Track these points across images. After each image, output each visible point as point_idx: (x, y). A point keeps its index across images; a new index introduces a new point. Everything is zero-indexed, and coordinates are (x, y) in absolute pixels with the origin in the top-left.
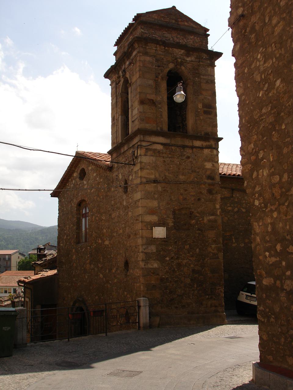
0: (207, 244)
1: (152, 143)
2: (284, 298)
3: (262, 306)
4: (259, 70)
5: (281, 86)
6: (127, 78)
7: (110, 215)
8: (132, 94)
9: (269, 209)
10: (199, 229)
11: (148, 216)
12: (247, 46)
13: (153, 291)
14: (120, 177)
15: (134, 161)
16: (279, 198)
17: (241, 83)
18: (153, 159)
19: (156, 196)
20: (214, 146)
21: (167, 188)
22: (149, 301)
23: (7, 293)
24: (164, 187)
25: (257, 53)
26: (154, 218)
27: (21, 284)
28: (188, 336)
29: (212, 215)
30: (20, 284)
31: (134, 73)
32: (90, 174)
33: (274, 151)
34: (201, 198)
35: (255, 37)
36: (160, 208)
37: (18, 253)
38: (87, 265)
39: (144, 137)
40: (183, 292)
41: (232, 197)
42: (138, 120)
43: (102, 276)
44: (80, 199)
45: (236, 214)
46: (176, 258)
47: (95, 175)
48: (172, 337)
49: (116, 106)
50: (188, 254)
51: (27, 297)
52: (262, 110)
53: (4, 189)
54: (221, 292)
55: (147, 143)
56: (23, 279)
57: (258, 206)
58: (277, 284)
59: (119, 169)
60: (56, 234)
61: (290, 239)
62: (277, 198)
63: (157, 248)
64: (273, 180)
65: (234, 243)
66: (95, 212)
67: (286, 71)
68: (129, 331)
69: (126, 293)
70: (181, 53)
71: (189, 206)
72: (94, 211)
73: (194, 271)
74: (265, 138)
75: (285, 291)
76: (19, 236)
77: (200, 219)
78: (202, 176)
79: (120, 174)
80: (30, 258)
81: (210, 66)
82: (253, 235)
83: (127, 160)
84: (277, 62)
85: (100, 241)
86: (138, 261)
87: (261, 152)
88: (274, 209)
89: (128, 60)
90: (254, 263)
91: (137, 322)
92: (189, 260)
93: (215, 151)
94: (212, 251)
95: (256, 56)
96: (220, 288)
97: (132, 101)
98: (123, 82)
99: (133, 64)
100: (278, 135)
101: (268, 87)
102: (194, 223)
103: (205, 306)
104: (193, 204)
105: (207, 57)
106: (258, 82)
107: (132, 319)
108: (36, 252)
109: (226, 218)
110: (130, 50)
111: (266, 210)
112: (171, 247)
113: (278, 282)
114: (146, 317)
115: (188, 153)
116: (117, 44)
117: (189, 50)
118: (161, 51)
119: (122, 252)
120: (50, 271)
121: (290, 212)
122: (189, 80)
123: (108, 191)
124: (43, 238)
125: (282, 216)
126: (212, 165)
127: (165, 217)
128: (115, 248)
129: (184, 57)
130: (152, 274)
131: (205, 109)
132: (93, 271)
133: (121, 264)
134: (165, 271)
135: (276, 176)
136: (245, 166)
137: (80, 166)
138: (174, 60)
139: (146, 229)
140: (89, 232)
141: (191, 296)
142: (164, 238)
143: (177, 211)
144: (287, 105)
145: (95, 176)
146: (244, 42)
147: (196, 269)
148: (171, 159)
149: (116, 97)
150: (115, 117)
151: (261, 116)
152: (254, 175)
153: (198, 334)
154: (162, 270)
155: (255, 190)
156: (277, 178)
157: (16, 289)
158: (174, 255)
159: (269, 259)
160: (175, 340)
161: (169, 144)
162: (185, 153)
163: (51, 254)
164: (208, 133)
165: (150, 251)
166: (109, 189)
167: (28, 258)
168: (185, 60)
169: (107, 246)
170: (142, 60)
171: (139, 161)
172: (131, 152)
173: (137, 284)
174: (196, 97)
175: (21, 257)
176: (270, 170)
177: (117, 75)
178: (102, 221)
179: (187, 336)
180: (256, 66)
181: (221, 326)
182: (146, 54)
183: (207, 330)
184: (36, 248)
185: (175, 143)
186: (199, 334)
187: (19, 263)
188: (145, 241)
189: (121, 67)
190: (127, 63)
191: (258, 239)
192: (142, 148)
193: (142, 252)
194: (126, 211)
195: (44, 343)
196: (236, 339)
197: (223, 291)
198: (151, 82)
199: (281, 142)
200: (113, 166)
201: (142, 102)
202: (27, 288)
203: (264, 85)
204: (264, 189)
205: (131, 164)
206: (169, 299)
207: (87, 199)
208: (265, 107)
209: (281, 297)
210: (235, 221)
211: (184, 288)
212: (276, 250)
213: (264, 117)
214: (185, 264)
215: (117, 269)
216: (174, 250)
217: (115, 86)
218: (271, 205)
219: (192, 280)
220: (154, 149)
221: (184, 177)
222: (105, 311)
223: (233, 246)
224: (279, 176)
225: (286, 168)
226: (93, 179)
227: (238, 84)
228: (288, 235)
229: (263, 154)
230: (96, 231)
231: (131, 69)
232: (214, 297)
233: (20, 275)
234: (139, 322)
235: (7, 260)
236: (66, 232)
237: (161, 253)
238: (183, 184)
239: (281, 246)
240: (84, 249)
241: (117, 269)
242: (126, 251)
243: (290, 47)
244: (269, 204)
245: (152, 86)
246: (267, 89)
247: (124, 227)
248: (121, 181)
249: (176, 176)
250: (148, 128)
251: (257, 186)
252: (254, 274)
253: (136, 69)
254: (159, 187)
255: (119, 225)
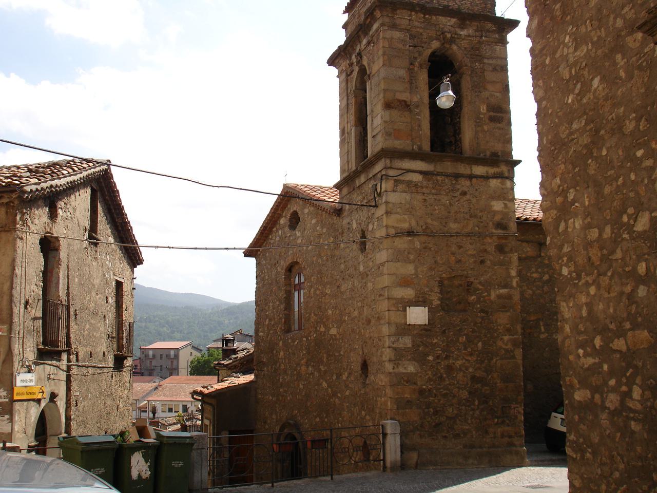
0: (496, 334)
1: (405, 171)
2: (606, 421)
3: (573, 433)
4: (567, 61)
5: (600, 88)
6: (364, 65)
7: (338, 287)
8: (373, 92)
9: (583, 281)
10: (482, 311)
11: (398, 289)
12: (549, 21)
13: (407, 410)
14: (355, 225)
15: (375, 199)
16: (598, 265)
17: (541, 81)
18: (407, 197)
19: (412, 257)
20: (506, 174)
21: (429, 243)
22: (400, 425)
23: (172, 412)
24: (424, 243)
25: (564, 35)
26: (409, 293)
27: (198, 398)
28: (463, 482)
29: (505, 287)
30: (195, 396)
31: (376, 58)
32: (306, 220)
33: (590, 189)
34: (486, 260)
35: (560, 9)
36: (417, 276)
37: (190, 347)
38: (302, 368)
39: (391, 161)
40: (455, 412)
41: (540, 256)
42: (383, 134)
43: (326, 385)
44: (290, 260)
45: (545, 285)
46: (445, 358)
47: (314, 221)
48: (437, 484)
49: (347, 111)
50: (464, 351)
51: (207, 418)
52: (572, 124)
53: (173, 248)
54: (519, 412)
55: (396, 171)
56: (199, 389)
57: (567, 276)
58: (595, 399)
59: (351, 212)
60: (252, 316)
61: (615, 329)
62: (596, 264)
63: (413, 341)
64: (589, 236)
65: (543, 333)
66: (315, 282)
67: (607, 64)
68: (368, 474)
69: (363, 413)
70: (452, 24)
71: (466, 273)
72: (312, 280)
73: (474, 378)
74: (577, 170)
75: (607, 411)
76: (192, 318)
77: (484, 294)
78: (487, 224)
79: (353, 221)
80: (210, 355)
81: (499, 43)
82: (560, 322)
83: (364, 198)
84: (594, 50)
85: (323, 329)
86: (384, 361)
87: (571, 191)
88: (591, 282)
89: (365, 36)
90: (561, 366)
91: (382, 460)
92: (466, 360)
93: (508, 183)
94: (504, 347)
95: (563, 39)
96: (518, 407)
97: (372, 104)
98: (358, 71)
99: (374, 43)
100: (596, 165)
101: (581, 89)
102: (475, 301)
103: (492, 436)
104: (472, 269)
105: (494, 29)
106: (565, 80)
107: (373, 454)
108: (219, 344)
109: (530, 292)
110: (368, 22)
111: (579, 282)
112: (437, 338)
113: (597, 396)
114: (396, 451)
115: (463, 186)
116: (348, 9)
117: (464, 18)
118: (419, 22)
119: (357, 347)
120: (244, 376)
121: (614, 287)
122: (465, 67)
123: (335, 248)
124: (231, 321)
125: (603, 292)
126: (503, 205)
127: (427, 291)
128: (346, 340)
129: (457, 30)
130: (405, 383)
131: (492, 114)
132: (311, 377)
133: (357, 366)
134: (427, 377)
135: (593, 230)
136: (547, 213)
137: (290, 208)
138: (440, 35)
139: (396, 310)
140: (305, 314)
141: (470, 418)
142: (425, 325)
143: (446, 281)
144: (610, 118)
145: (314, 224)
146: (545, 15)
147: (478, 375)
148: (435, 196)
149: (348, 96)
150: (346, 129)
151: (571, 133)
152: (560, 227)
153: (479, 480)
154: (421, 376)
155: (563, 251)
156: (594, 234)
157: (186, 406)
158: (441, 352)
159: (585, 360)
160: (441, 489)
161: (432, 171)
162: (458, 187)
163: (245, 349)
164: (498, 153)
165: (401, 346)
166: (337, 246)
167: (207, 355)
168: (458, 34)
169: (334, 337)
170: (388, 37)
171: (383, 202)
172: (370, 186)
173: (381, 399)
174: (476, 94)
175: (195, 353)
176: (585, 219)
177: (348, 62)
178: (325, 296)
179: (461, 483)
180: (563, 54)
181: (518, 469)
182: (394, 26)
183: (495, 475)
184: (219, 338)
185: (442, 171)
186: (481, 480)
187: (192, 362)
188: (393, 329)
189: (355, 48)
190: (365, 42)
191: (567, 328)
192: (388, 179)
193: (389, 347)
194: (364, 281)
195: (234, 488)
196: (541, 489)
197: (522, 412)
198: (402, 73)
199: (600, 175)
200: (343, 209)
201: (388, 106)
202: (208, 403)
203: (575, 85)
204: (576, 249)
205: (371, 206)
206: (434, 424)
207: (301, 260)
208: (577, 121)
209: (601, 419)
210: (545, 296)
211: (458, 406)
212: (594, 346)
213: (576, 135)
214: (458, 367)
215: (350, 374)
216: (441, 345)
217: (345, 77)
218: (587, 275)
219: (470, 393)
220: (408, 181)
221: (456, 225)
222: (330, 441)
223: (541, 337)
224: (598, 229)
225: (608, 218)
226: (310, 229)
227: (535, 82)
228: (611, 323)
229: (575, 194)
230: (316, 313)
231: (371, 52)
232: (507, 422)
233: (193, 382)
234: (384, 460)
235: (171, 359)
236: (269, 313)
237: (420, 349)
238: (455, 238)
239: (602, 340)
240: (297, 341)
241: (350, 374)
242: (364, 345)
243: (612, 27)
244: (583, 274)
245: (404, 79)
246: (580, 92)
247: (361, 307)
248: (356, 233)
249: (444, 224)
250: (398, 147)
251: (566, 246)
252: (561, 383)
253: (378, 51)
254: (416, 242)
255: (352, 303)
